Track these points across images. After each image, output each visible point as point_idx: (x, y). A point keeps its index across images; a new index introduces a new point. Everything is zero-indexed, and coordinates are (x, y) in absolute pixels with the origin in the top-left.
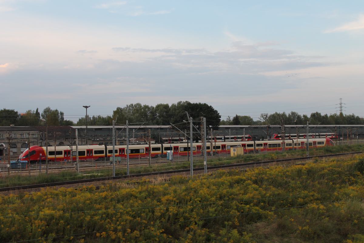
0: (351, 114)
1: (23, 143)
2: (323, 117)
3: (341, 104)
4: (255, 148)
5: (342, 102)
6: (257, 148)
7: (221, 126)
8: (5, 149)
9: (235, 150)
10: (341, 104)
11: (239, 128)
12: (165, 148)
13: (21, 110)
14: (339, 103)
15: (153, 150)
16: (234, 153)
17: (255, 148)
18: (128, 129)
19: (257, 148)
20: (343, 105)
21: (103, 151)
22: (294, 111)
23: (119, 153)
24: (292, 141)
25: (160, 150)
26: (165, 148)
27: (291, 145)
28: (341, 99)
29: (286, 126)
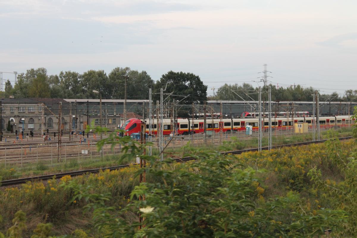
0: (309, 88)
1: (30, 118)
2: (278, 90)
3: (265, 72)
4: (336, 123)
5: (268, 70)
6: (234, 127)
7: (209, 102)
8: (16, 124)
9: (301, 125)
10: (265, 72)
11: (117, 104)
12: (234, 123)
13: (325, 90)
14: (263, 70)
15: (225, 125)
16: (300, 130)
17: (336, 123)
18: (270, 104)
19: (234, 127)
20: (268, 74)
21: (198, 124)
22: (246, 83)
23: (200, 127)
24: (334, 117)
25: (239, 125)
26: (234, 123)
27: (187, 127)
28: (265, 65)
29: (67, 100)
